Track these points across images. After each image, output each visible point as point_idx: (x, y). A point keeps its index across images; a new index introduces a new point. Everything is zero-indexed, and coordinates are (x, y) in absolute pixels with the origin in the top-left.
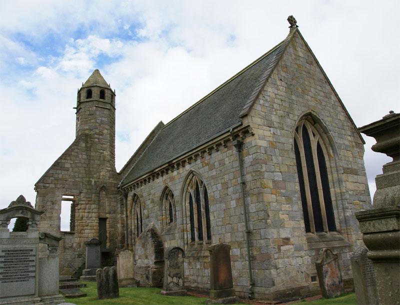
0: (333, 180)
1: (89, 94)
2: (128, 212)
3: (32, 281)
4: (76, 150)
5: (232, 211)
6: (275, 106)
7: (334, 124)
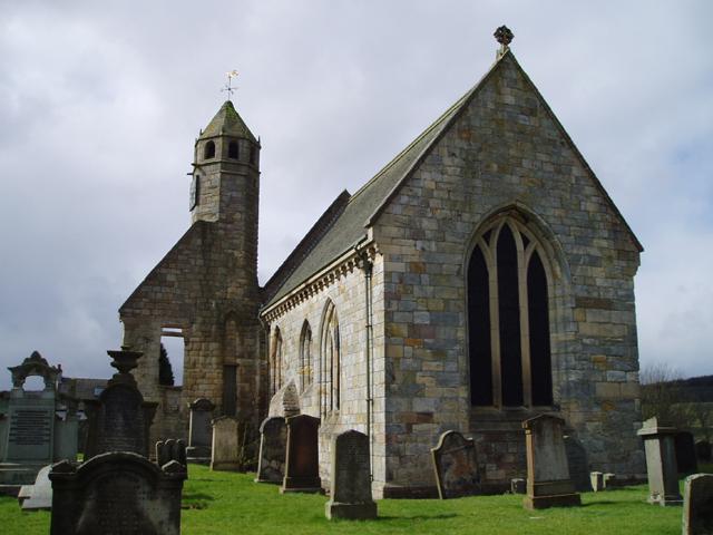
3: (46, 445)
4: (186, 252)
6: (433, 203)
7: (567, 221)
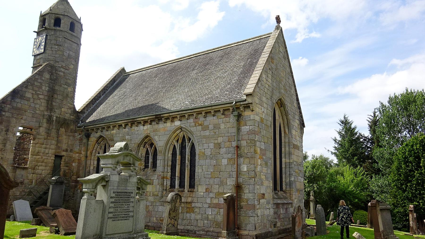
0: (285, 152)
1: (57, 22)
2: (89, 152)
4: (39, 81)
5: (325, 174)
